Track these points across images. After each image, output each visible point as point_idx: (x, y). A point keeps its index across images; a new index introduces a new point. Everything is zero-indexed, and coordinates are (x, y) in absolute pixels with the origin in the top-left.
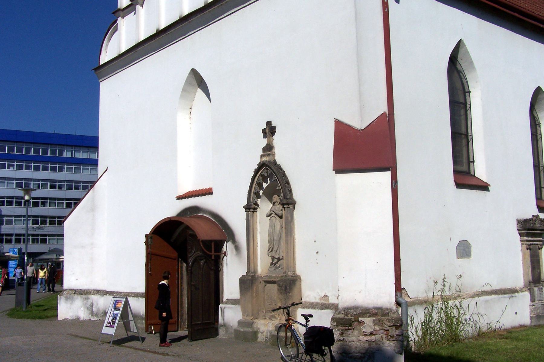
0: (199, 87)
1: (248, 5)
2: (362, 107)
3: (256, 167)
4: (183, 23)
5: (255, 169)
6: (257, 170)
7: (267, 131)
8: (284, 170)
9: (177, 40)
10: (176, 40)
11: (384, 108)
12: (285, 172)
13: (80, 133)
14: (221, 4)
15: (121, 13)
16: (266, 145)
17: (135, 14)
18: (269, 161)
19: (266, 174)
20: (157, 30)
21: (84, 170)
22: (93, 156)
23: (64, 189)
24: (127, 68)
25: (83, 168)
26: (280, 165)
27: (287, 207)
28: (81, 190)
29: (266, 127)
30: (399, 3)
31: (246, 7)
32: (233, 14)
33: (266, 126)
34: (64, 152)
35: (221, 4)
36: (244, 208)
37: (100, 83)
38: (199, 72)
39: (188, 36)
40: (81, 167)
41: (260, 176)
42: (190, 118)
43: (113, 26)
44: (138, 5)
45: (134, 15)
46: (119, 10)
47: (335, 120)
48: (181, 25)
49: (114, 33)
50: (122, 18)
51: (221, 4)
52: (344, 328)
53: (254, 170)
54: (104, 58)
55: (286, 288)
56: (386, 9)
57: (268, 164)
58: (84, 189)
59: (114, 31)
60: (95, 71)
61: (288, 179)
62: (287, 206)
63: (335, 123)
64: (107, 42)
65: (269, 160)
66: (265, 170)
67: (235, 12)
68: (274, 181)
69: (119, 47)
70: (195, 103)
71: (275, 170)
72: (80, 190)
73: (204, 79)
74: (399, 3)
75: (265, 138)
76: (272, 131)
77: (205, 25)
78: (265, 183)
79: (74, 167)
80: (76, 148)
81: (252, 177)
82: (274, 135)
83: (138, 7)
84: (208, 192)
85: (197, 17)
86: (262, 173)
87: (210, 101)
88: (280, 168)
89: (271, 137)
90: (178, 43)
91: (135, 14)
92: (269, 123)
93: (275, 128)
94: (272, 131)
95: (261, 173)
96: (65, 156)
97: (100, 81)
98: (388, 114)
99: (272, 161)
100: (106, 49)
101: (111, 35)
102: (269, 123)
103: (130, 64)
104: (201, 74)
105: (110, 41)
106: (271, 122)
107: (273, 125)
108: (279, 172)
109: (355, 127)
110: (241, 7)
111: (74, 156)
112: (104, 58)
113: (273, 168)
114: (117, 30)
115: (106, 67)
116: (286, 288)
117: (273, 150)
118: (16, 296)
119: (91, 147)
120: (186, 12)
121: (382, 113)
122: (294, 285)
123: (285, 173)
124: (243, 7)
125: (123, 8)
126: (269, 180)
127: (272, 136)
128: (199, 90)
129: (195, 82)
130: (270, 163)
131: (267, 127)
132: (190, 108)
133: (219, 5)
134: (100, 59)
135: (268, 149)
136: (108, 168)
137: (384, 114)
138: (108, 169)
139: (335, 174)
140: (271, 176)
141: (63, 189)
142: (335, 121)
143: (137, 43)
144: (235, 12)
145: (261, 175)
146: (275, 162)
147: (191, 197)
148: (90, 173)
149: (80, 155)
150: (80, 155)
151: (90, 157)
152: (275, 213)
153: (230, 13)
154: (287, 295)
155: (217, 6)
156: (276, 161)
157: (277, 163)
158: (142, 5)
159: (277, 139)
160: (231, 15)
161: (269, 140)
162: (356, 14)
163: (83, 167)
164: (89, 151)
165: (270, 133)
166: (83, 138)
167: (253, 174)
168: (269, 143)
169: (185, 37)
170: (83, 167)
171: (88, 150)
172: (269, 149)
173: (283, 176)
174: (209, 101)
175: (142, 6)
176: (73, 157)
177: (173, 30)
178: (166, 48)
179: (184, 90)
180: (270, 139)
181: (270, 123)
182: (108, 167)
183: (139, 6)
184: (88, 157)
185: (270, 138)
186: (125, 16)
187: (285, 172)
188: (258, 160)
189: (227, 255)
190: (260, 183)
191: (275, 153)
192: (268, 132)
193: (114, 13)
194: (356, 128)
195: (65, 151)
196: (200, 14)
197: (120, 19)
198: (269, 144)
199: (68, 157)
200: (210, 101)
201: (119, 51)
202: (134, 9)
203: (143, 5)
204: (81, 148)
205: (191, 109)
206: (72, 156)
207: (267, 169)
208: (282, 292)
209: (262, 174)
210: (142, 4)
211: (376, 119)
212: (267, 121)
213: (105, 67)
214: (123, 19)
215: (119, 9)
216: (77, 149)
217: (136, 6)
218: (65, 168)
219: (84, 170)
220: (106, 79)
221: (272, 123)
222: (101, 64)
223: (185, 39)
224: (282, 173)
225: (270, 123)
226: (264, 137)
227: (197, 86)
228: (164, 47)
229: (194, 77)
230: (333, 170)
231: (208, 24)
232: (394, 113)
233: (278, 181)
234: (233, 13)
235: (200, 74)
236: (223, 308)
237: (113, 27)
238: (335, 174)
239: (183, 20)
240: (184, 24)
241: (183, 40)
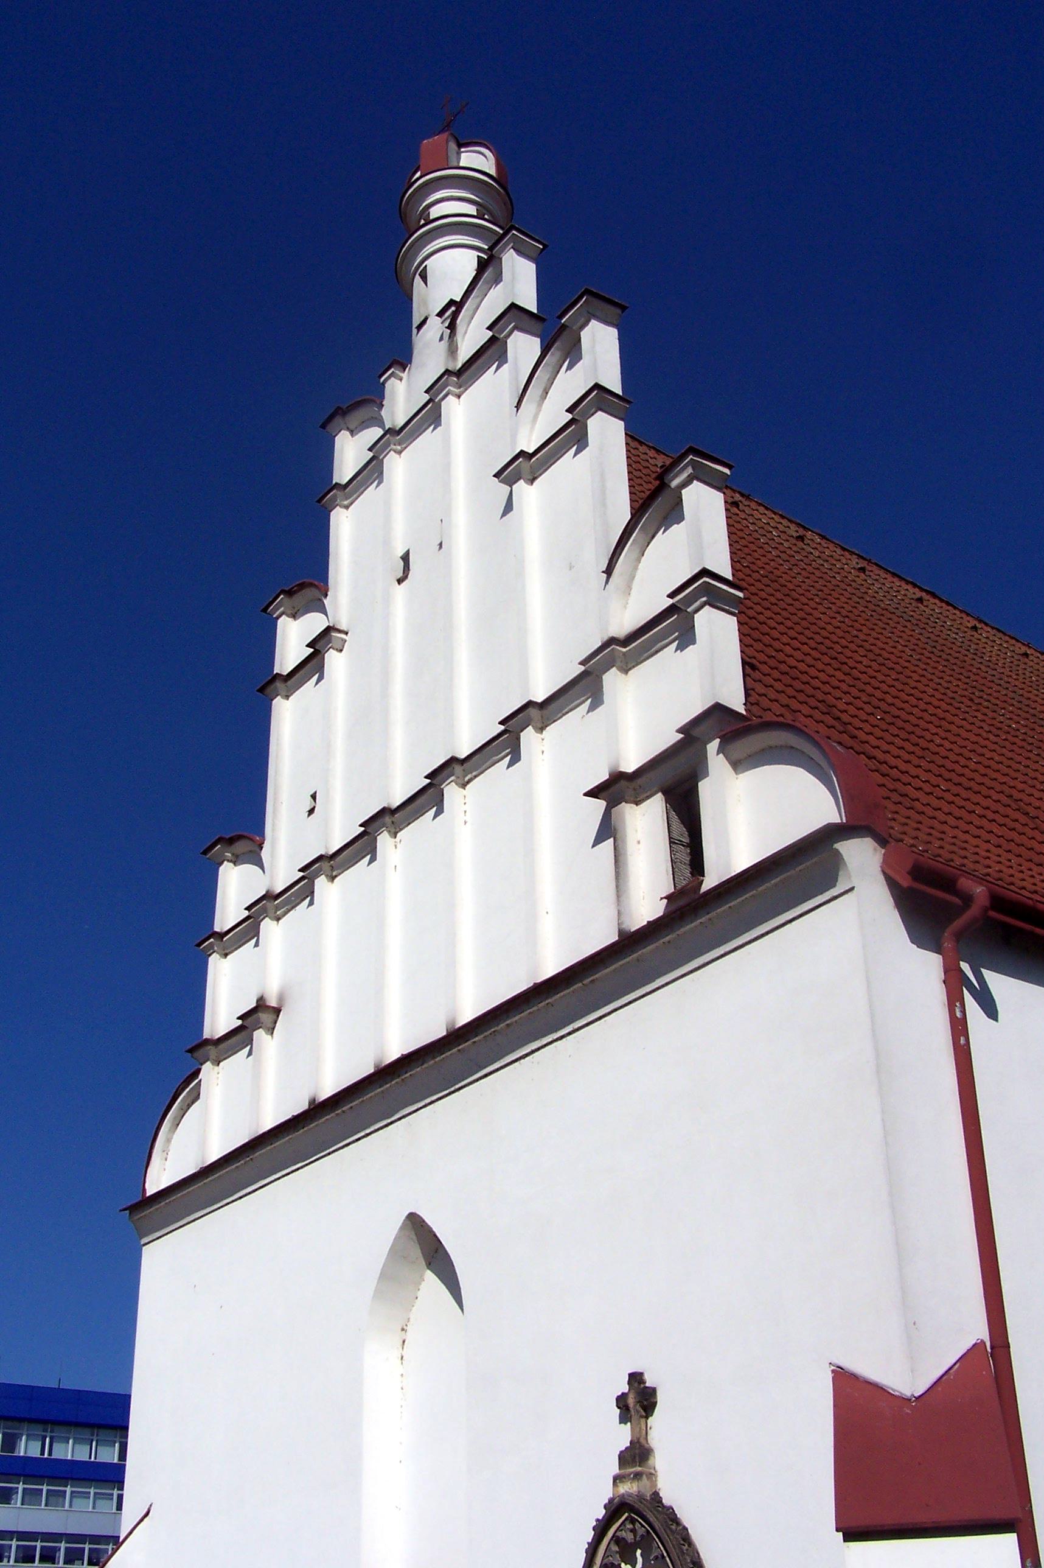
0: (429, 1265)
1: (569, 1034)
2: (911, 1327)
3: (601, 1513)
4: (387, 1084)
5: (597, 1520)
6: (602, 1524)
7: (631, 1401)
8: (686, 1526)
9: (368, 1131)
10: (364, 1129)
11: (979, 1330)
12: (687, 1529)
13: (71, 1383)
14: (493, 1030)
15: (212, 1051)
16: (629, 1445)
17: (250, 1054)
18: (640, 1497)
19: (630, 1537)
20: (312, 1102)
21: (75, 1500)
22: (108, 1455)
23: (9, 1562)
24: (222, 1207)
25: (72, 1492)
26: (673, 1509)
28: (61, 1564)
29: (626, 1391)
30: (997, 1020)
31: (564, 1040)
32: (526, 1059)
33: (627, 1387)
34: (21, 1440)
35: (493, 1030)
37: (144, 1248)
38: (429, 1224)
39: (400, 1119)
40: (68, 1489)
41: (612, 1542)
42: (402, 1358)
43: (187, 1088)
44: (261, 1030)
45: (248, 1056)
46: (207, 1042)
47: (833, 1368)
48: (380, 1087)
49: (189, 1106)
50: (213, 1064)
51: (494, 1031)
53: (595, 1523)
54: (158, 1178)
56: (962, 1038)
57: (636, 1506)
58: (68, 1561)
59: (189, 1101)
60: (130, 1213)
61: (698, 1553)
63: (833, 1378)
64: (170, 1130)
65: (639, 1492)
66: (627, 1522)
67: (533, 1052)
68: (656, 1558)
69: (203, 1143)
70: (417, 1313)
71: (657, 1525)
72: (58, 1563)
73: (443, 1243)
74: (997, 1020)
75: (625, 1423)
76: (645, 1403)
77: (449, 1088)
78: (628, 1566)
79: (45, 1488)
80: (57, 1428)
81: (587, 1546)
82: (652, 1415)
83: (259, 1035)
85: (425, 1065)
86: (619, 1534)
87: (462, 1310)
88: (672, 1516)
89: (643, 1421)
90: (370, 1137)
91: (250, 1054)
92: (636, 1378)
93: (653, 1391)
94: (645, 1403)
95: (616, 1532)
96: (22, 1454)
97: (142, 1243)
98: (992, 1348)
99: (648, 1495)
100: (165, 1151)
101: (182, 1113)
102: (636, 1378)
103: (232, 1195)
104: (434, 1229)
105: (177, 1128)
106: (641, 1374)
107: (647, 1385)
108: (669, 1532)
109: (894, 1390)
110: (550, 1040)
111: (50, 1453)
112: (158, 1178)
113: (652, 1519)
114: (197, 1097)
115: (163, 1203)
117: (650, 1462)
119: (100, 1426)
120: (393, 1054)
121: (974, 1342)
123: (688, 1533)
124: (555, 1038)
125: (217, 1037)
126: (642, 1555)
127: (647, 1418)
128: (430, 1276)
129: (416, 1252)
130: (641, 1502)
131: (629, 1390)
132: (403, 1329)
133: (486, 1034)
134: (147, 1180)
136: (153, 1505)
137: (978, 1346)
138: (151, 1512)
139: (845, 1541)
140: (644, 1541)
141: (5, 1560)
142: (833, 1371)
143: (253, 1137)
144: (533, 1052)
145: (616, 1540)
146: (656, 1497)
148: (94, 1508)
149: (69, 1450)
150: (69, 1450)
151: (95, 1458)
153: (518, 1056)
155: (482, 1036)
156: (658, 1494)
157: (664, 1501)
158: (271, 1030)
159: (658, 1423)
160: (522, 1061)
161: (638, 1430)
162: (878, 1054)
163: (74, 1489)
164: (95, 1438)
165: (638, 1407)
166: (79, 1397)
167: (589, 1535)
168: (638, 1439)
169: (392, 1123)
170: (74, 1489)
171: (93, 1435)
172: (637, 1458)
173: (682, 1542)
174: (457, 1306)
175: (272, 1033)
176: (46, 1455)
177: (357, 1102)
178: (336, 1153)
179: (385, 1276)
180: (640, 1428)
181: (638, 1378)
182: (151, 1505)
183: (263, 1032)
184: (90, 1458)
185: (639, 1423)
186: (222, 1058)
187: (689, 1530)
188: (606, 1492)
190: (613, 1564)
191: (656, 1472)
192: (635, 1406)
193: (191, 1051)
194: (897, 1393)
195: (24, 1438)
196: (434, 1058)
197: (207, 1067)
198: (638, 1442)
199: (29, 1455)
200: (462, 1310)
201: (203, 1160)
202: (250, 1041)
203: (273, 1029)
204: (73, 1429)
205: (404, 1332)
206: (43, 1453)
207: (633, 1521)
209: (618, 1537)
210: (271, 1026)
211: (955, 1364)
212: (631, 1372)
213: (160, 1203)
214: (216, 1068)
215: (206, 1039)
216: (59, 1431)
217: (256, 1033)
218: (17, 1492)
219: (75, 1500)
220: (160, 1237)
221: (646, 1377)
222: (148, 1194)
223: (390, 1127)
224: (678, 1534)
225: (638, 1378)
226: (623, 1419)
227: (426, 1267)
228: (331, 1150)
229: (414, 1237)
230: (837, 1530)
231: (457, 1086)
232: (1009, 1343)
233: (668, 1559)
234: (527, 1055)
235: (431, 1228)
237: (187, 1090)
238: (845, 1541)
239: (385, 1074)
240: (388, 1085)
241: (385, 1129)
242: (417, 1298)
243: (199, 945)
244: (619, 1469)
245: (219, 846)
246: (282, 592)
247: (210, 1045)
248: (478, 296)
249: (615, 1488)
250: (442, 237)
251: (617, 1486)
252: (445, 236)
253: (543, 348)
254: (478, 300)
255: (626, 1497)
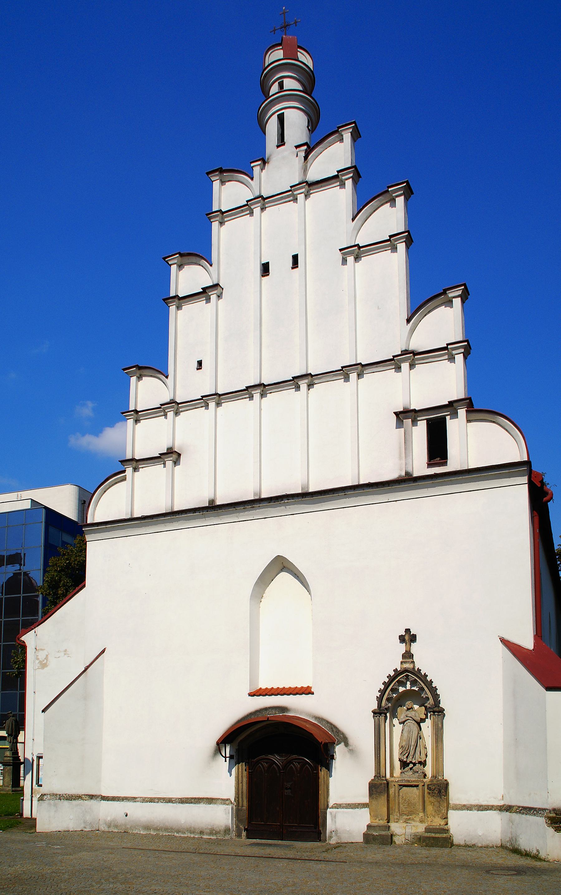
27: (438, 715)
30: (394, 413)
36: (372, 712)
49: (113, 485)
52: (557, 825)
55: (440, 792)
62: (437, 714)
84: (307, 691)
116: (440, 792)
118: (29, 818)
122: (376, 784)
135: (408, 655)
147: (276, 695)
152: (413, 719)
154: (441, 798)
189: (336, 758)
208: (433, 796)
236: (335, 812)
242: (261, 602)
243: (123, 413)
244: (402, 659)
245: (135, 369)
246: (179, 253)
247: (134, 461)
248: (323, 148)
249: (402, 665)
250: (274, 106)
251: (403, 664)
252: (276, 105)
253: (306, 154)
254: (322, 149)
255: (407, 668)
